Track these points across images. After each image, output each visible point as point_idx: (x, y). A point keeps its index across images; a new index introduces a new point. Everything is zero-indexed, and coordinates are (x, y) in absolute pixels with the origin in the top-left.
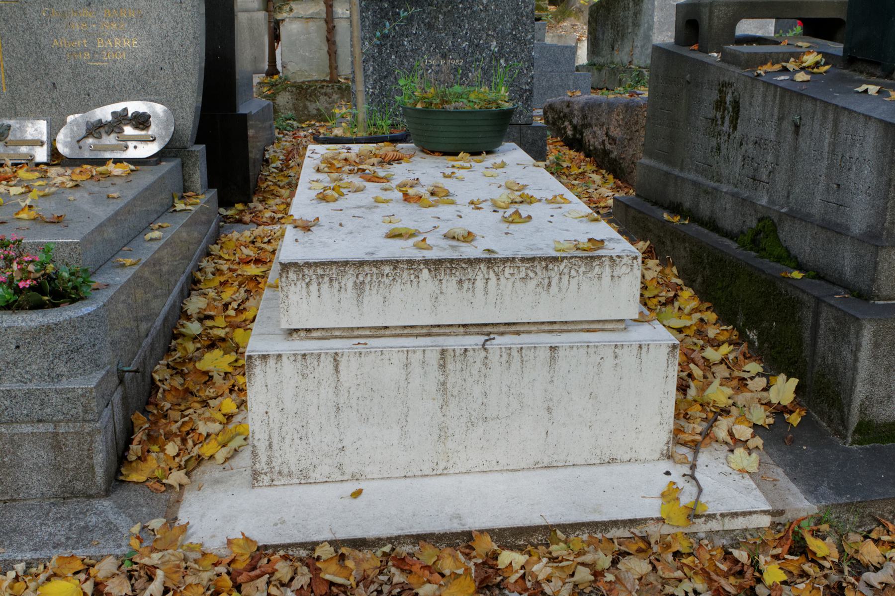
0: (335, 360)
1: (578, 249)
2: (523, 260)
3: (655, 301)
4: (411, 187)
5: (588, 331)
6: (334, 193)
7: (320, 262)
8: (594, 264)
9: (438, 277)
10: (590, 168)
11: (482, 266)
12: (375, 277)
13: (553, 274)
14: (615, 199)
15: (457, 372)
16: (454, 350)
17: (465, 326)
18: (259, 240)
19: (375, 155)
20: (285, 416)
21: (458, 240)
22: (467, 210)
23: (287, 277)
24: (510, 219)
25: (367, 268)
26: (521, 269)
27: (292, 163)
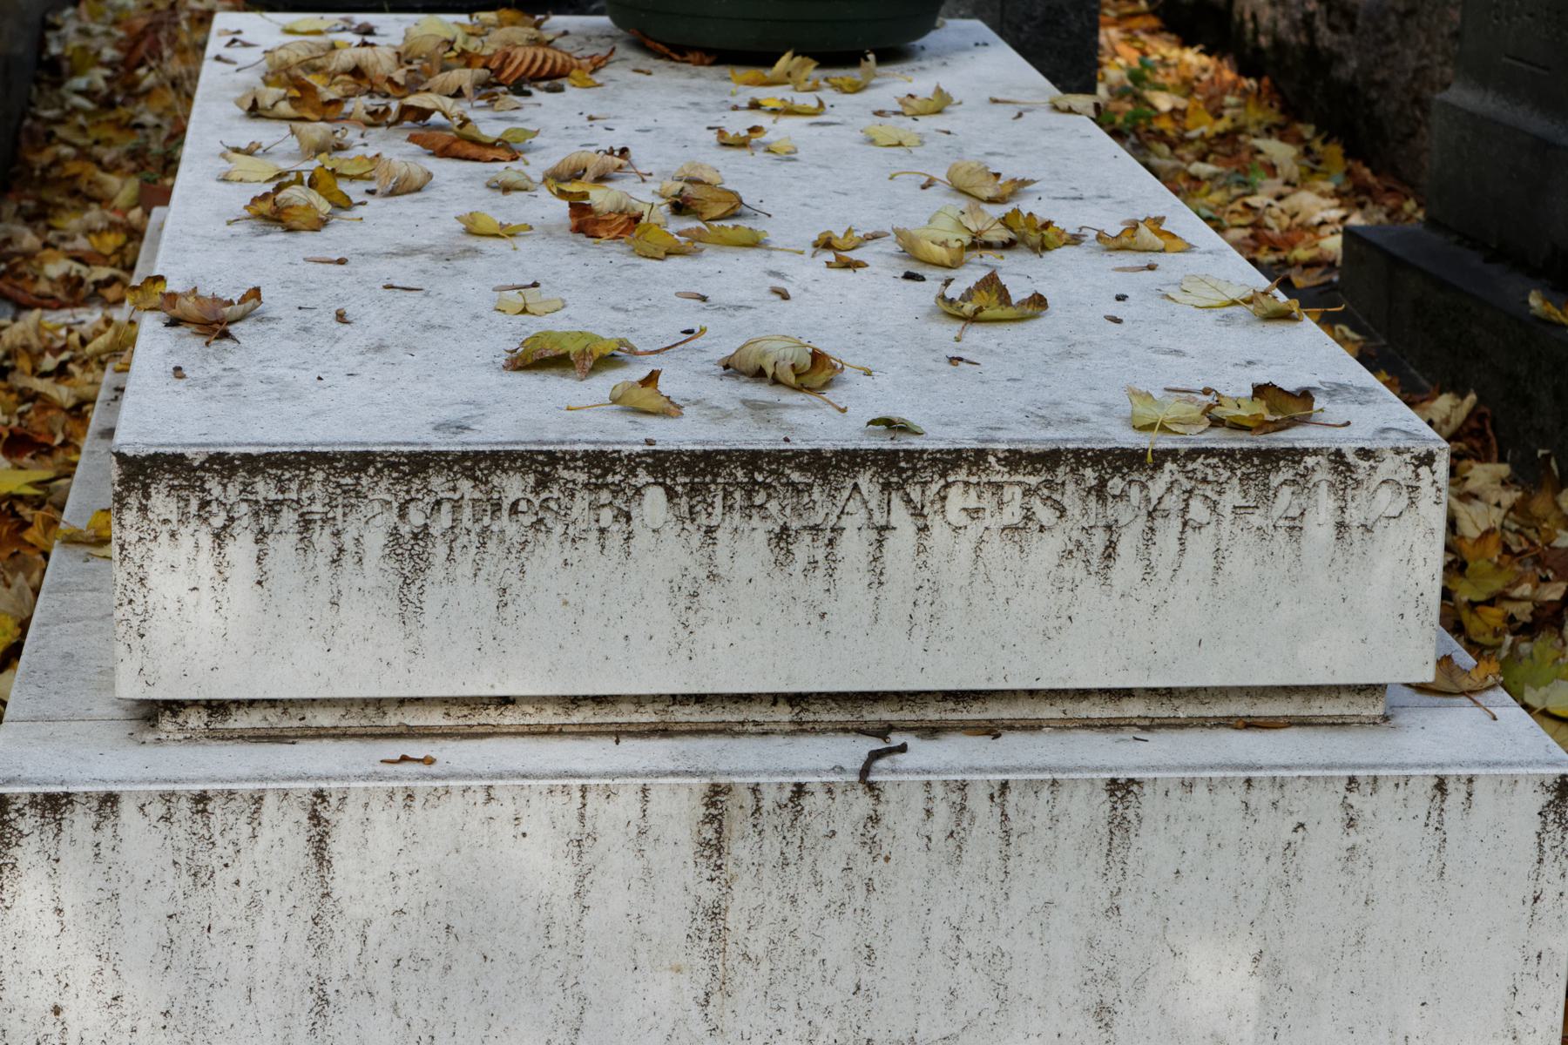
0: (315, 817)
1: (1216, 423)
2: (1015, 460)
3: (1494, 615)
4: (601, 178)
5: (1250, 724)
6: (315, 197)
7: (155, 458)
8: (1275, 480)
9: (703, 519)
10: (1254, 115)
11: (864, 480)
12: (467, 513)
13: (1121, 513)
14: (1350, 235)
15: (766, 872)
16: (755, 789)
17: (796, 700)
18: (24, 363)
19: (466, 59)
20: (126, 1025)
21: (776, 381)
22: (810, 272)
23: (143, 509)
24: (969, 308)
25: (438, 482)
26: (1008, 492)
27: (147, 77)
